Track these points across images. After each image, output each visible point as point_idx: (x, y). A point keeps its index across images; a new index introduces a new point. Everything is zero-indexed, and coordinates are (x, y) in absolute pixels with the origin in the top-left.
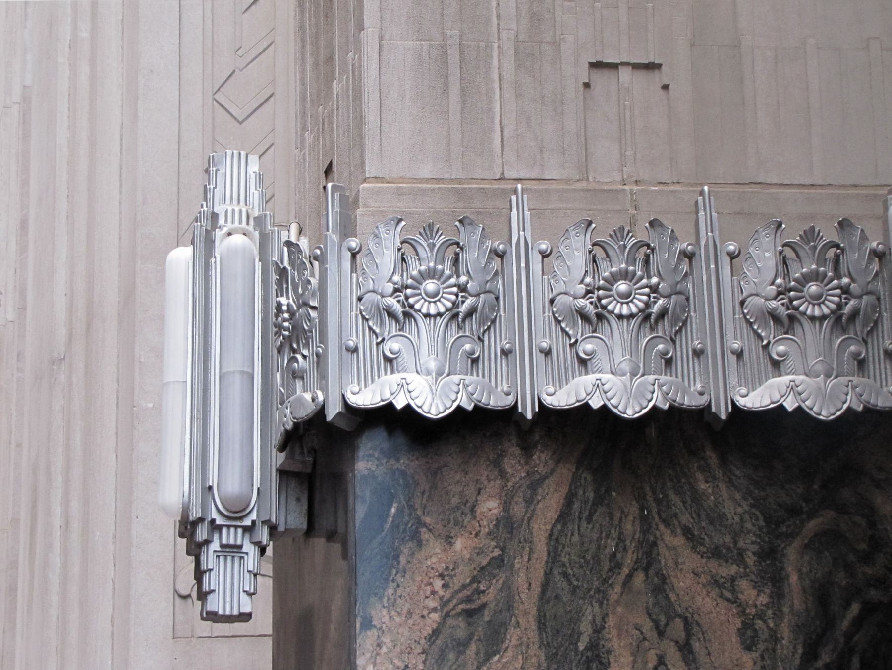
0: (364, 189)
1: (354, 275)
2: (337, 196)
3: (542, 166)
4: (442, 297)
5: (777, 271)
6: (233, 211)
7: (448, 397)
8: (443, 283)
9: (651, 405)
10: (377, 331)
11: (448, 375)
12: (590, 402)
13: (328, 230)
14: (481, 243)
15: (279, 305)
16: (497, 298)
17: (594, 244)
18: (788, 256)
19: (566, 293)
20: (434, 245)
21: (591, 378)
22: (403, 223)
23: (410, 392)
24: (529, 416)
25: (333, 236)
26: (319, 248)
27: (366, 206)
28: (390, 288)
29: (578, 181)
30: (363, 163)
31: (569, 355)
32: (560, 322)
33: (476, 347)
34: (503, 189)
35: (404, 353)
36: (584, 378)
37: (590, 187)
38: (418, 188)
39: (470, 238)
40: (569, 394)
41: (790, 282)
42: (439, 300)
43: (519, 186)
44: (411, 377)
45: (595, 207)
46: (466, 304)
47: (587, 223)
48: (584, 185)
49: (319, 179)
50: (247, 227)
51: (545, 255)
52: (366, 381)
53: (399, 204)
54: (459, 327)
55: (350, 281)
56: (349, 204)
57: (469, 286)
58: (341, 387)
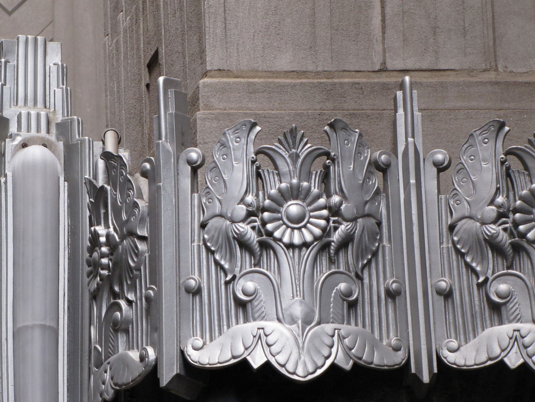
0: (205, 85)
1: (196, 195)
2: (171, 93)
3: (437, 52)
4: (308, 222)
5: (248, 185)
6: (29, 114)
7: (319, 352)
8: (309, 204)
9: (328, 363)
10: (227, 266)
11: (319, 323)
12: (506, 360)
13: (160, 138)
14: (358, 153)
15: (95, 236)
16: (379, 224)
17: (507, 153)
18: (513, 168)
19: (470, 217)
20: (298, 156)
21: (507, 329)
22: (258, 128)
23: (269, 346)
24: (426, 379)
25: (167, 145)
26: (149, 161)
27: (207, 107)
28: (241, 210)
29: (484, 71)
30: (202, 52)
31: (476, 299)
32: (463, 255)
33: (353, 287)
34: (384, 84)
35: (262, 296)
36: (498, 329)
37: (500, 78)
38: (275, 84)
39: (343, 146)
40: (477, 351)
41: (515, 201)
42: (305, 226)
43: (407, 79)
44: (271, 325)
45: (507, 105)
46: (339, 231)
47: (498, 126)
48: (491, 76)
49: (140, 75)
50: (47, 136)
51: (441, 168)
52: (212, 333)
53: (250, 105)
54: (331, 262)
55: (190, 201)
56: (187, 104)
57: (343, 207)
58: (179, 342)
